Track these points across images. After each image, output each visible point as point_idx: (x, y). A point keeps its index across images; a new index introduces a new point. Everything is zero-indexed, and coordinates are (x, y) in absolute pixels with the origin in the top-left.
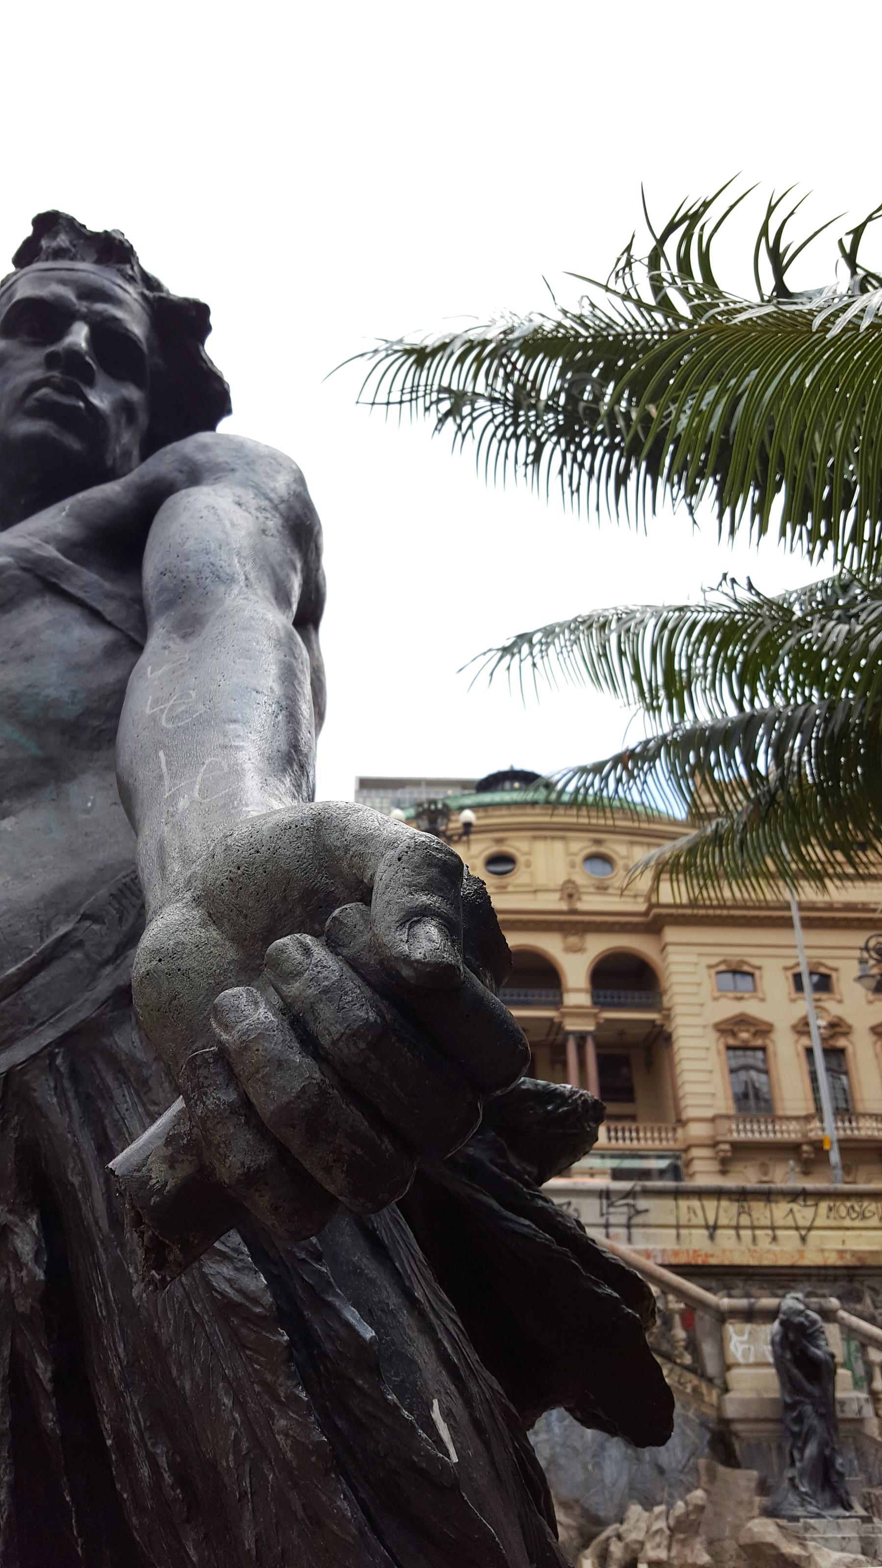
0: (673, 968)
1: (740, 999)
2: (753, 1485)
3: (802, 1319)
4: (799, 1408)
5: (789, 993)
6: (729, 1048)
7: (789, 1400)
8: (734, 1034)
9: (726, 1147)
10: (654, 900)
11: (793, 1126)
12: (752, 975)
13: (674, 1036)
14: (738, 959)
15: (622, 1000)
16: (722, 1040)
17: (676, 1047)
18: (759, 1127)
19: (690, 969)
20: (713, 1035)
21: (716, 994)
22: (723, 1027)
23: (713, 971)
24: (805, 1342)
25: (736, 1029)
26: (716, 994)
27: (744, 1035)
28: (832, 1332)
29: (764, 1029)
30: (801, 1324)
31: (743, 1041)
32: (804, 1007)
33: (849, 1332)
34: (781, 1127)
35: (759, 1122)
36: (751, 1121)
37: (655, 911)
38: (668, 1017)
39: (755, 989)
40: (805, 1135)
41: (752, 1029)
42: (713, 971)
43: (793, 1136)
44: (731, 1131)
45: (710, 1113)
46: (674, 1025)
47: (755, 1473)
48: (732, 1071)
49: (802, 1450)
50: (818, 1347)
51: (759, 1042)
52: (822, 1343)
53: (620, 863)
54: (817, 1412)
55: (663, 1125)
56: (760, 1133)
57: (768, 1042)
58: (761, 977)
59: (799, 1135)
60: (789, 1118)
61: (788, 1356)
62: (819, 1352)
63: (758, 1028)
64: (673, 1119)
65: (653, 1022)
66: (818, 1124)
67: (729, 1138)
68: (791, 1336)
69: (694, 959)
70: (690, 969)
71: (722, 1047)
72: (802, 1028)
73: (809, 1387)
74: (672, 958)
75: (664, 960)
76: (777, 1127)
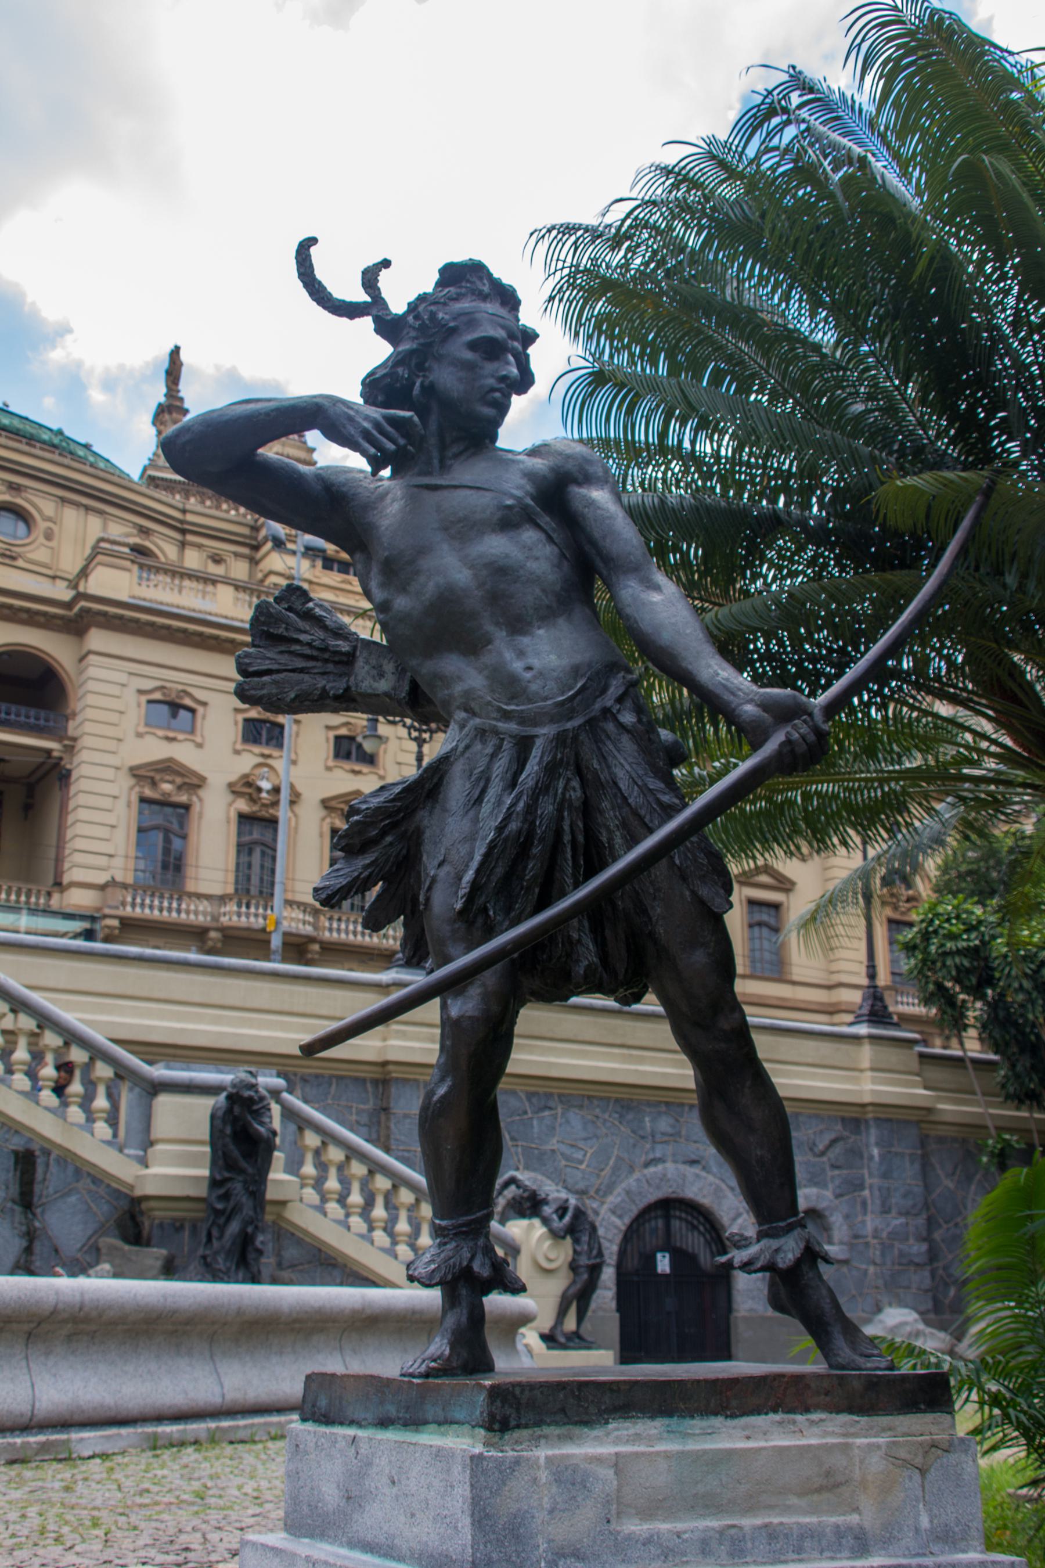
0: (91, 685)
1: (170, 739)
2: (159, 1264)
3: (252, 1093)
4: (229, 1185)
5: (235, 743)
6: (143, 800)
7: (218, 1177)
8: (154, 784)
9: (115, 923)
10: (81, 589)
11: (204, 906)
12: (193, 711)
13: (74, 775)
14: (180, 687)
15: (13, 717)
16: (137, 789)
17: (73, 790)
18: (161, 903)
19: (115, 690)
20: (126, 782)
21: (142, 729)
22: (142, 772)
23: (144, 699)
24: (249, 1118)
25: (158, 777)
26: (142, 729)
27: (167, 787)
28: (276, 1109)
29: (194, 782)
30: (251, 1099)
31: (164, 794)
32: (246, 762)
33: (289, 1113)
34: (188, 905)
35: (162, 897)
36: (153, 895)
37: (83, 604)
38: (70, 749)
39: (192, 731)
40: (215, 918)
41: (179, 780)
42: (144, 699)
43: (201, 918)
44: (124, 904)
45: (102, 878)
46: (76, 760)
47: (164, 1252)
48: (141, 830)
49: (222, 1229)
50: (262, 1123)
51: (183, 798)
52: (267, 1120)
53: (42, 525)
54: (247, 1189)
55: (34, 888)
56: (161, 910)
57: (195, 798)
58: (204, 717)
59: (209, 918)
60: (199, 896)
61: (228, 1130)
62: (262, 1129)
63: (187, 780)
64: (51, 880)
65: (48, 752)
66: (235, 908)
67: (120, 912)
68: (237, 1110)
69: (123, 678)
70: (115, 690)
71: (135, 798)
72: (245, 787)
73: (243, 1164)
74: (92, 672)
75: (81, 672)
76: (184, 906)
